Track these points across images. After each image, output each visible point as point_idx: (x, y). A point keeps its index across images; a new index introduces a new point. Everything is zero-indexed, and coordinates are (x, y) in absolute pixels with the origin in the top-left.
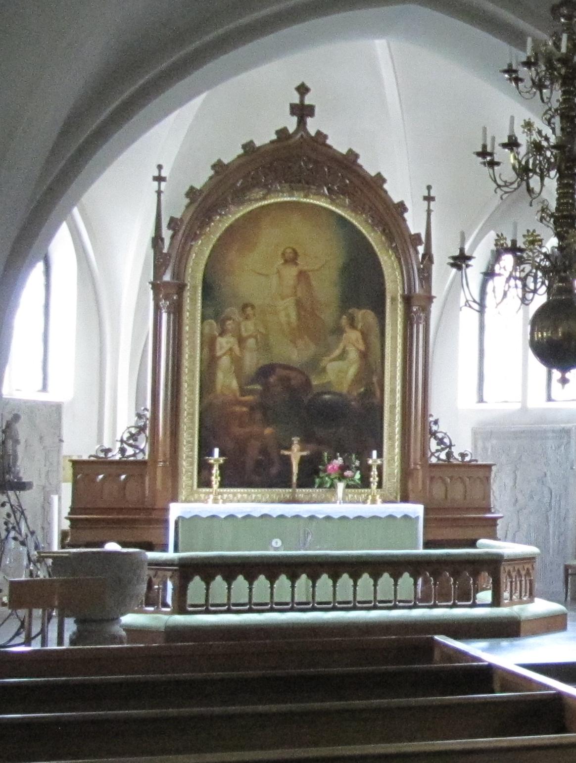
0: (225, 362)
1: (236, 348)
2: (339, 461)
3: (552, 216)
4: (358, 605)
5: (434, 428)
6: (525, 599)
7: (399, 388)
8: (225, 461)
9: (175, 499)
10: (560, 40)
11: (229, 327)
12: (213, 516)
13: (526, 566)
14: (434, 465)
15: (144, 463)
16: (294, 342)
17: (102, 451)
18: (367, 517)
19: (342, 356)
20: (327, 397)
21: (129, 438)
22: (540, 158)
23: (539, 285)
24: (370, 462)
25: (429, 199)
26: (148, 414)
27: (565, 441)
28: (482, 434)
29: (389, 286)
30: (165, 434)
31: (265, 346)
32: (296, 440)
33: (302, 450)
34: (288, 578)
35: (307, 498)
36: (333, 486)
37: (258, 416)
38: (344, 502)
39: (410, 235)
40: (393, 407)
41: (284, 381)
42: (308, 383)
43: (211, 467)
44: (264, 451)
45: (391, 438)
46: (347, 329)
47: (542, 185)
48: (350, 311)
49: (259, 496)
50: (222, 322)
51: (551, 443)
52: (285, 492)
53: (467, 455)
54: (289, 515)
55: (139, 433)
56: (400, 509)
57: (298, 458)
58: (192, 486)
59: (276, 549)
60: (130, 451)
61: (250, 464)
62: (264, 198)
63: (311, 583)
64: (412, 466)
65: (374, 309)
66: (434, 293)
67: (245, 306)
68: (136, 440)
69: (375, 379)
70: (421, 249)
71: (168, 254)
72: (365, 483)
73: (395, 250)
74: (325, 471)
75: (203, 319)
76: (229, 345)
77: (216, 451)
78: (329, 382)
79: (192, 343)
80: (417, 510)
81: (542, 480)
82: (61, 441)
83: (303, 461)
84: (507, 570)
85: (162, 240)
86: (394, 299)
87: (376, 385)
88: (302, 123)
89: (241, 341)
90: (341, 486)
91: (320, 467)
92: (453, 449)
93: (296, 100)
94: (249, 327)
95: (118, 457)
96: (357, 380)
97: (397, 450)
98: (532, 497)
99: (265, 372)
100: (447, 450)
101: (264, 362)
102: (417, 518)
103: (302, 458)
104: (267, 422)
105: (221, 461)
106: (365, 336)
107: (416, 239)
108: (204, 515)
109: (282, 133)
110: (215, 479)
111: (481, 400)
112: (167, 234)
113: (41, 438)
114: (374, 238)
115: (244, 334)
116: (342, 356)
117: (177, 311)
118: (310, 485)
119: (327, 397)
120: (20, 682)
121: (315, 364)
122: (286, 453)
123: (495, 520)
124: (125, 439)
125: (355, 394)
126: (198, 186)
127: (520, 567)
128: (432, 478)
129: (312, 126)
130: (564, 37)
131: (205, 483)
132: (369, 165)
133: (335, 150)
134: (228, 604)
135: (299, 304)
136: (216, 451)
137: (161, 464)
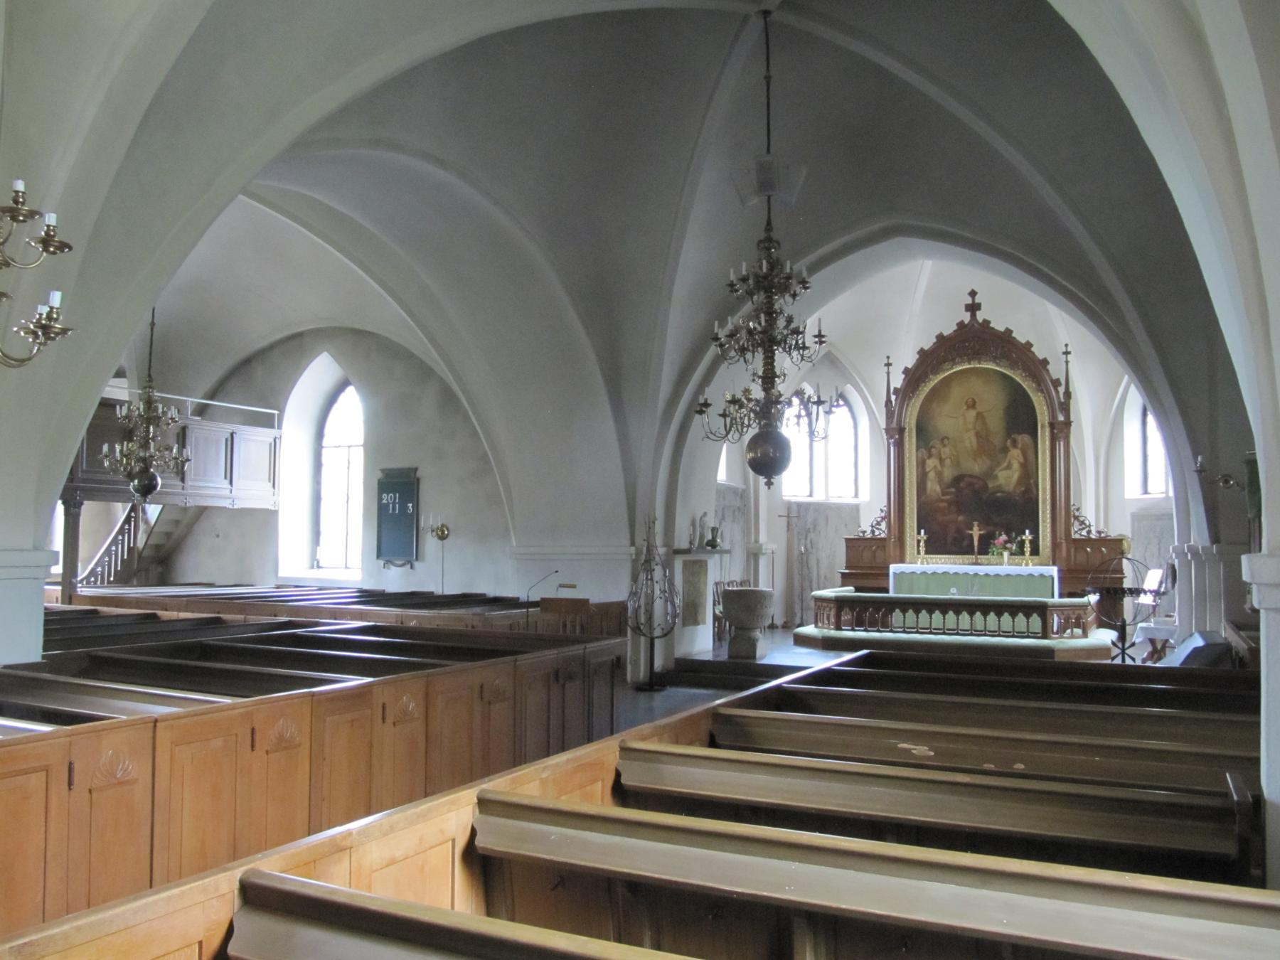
0: (932, 475)
3: (759, 377)
4: (987, 633)
5: (1077, 514)
8: (927, 538)
9: (902, 561)
10: (762, 264)
12: (913, 573)
14: (1075, 540)
16: (975, 460)
18: (992, 574)
19: (1009, 467)
22: (800, 339)
23: (752, 422)
28: (1138, 518)
30: (895, 520)
31: (956, 463)
33: (980, 530)
34: (1039, 616)
36: (1002, 554)
38: (1010, 564)
41: (970, 485)
42: (986, 486)
44: (959, 531)
46: (1011, 449)
47: (753, 357)
48: (1013, 436)
50: (929, 451)
52: (972, 558)
55: (882, 521)
58: (914, 553)
59: (953, 594)
60: (877, 533)
61: (949, 540)
62: (952, 368)
63: (956, 618)
64: (1058, 540)
65: (1029, 434)
66: (1072, 419)
67: (942, 440)
68: (880, 525)
69: (1032, 481)
70: (1062, 390)
73: (1042, 391)
77: (1027, 532)
83: (981, 537)
86: (1043, 426)
87: (1033, 485)
88: (973, 316)
89: (941, 460)
90: (1006, 554)
93: (969, 301)
94: (946, 451)
95: (869, 536)
96: (1020, 482)
99: (958, 480)
100: (1088, 529)
101: (956, 474)
103: (980, 535)
104: (960, 512)
105: (925, 538)
106: (1024, 453)
107: (1056, 383)
109: (961, 325)
110: (922, 549)
111: (1146, 492)
112: (893, 398)
113: (846, 525)
114: (1028, 386)
115: (943, 457)
116: (1009, 467)
117: (900, 445)
118: (986, 553)
119: (999, 494)
120: (864, 671)
121: (990, 474)
122: (970, 532)
125: (1018, 491)
126: (910, 366)
129: (980, 316)
130: (764, 262)
132: (1020, 336)
133: (996, 330)
134: (904, 627)
135: (978, 435)
136: (1027, 532)
137: (893, 540)
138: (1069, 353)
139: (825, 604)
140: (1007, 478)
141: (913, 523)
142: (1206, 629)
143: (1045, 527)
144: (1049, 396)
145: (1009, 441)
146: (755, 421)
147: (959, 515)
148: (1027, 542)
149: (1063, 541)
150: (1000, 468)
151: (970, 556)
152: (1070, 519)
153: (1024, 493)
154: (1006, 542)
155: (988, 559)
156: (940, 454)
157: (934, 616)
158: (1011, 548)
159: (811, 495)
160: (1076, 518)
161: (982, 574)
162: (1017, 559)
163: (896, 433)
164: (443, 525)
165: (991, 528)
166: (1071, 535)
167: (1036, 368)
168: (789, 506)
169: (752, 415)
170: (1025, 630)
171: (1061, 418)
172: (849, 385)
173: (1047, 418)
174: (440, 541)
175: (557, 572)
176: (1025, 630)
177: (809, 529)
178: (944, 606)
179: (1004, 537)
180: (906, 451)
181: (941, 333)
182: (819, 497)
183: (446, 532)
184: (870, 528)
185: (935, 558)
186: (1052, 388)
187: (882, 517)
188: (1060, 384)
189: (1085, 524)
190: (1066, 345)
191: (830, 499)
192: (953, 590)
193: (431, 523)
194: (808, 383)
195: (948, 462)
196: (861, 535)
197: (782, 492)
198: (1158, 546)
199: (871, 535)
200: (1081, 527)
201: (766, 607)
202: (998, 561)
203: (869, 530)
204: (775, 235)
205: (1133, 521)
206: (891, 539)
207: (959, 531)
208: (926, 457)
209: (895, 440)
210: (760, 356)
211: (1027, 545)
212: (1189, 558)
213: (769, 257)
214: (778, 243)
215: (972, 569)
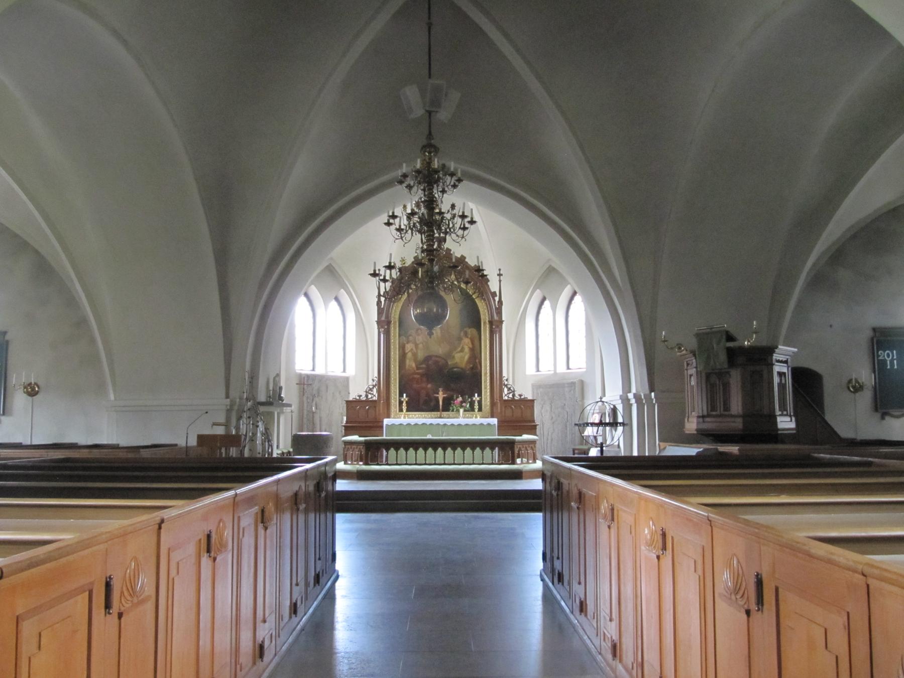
0: (409, 355)
1: (414, 349)
2: (460, 399)
5: (506, 383)
6: (531, 462)
7: (488, 364)
9: (388, 417)
11: (411, 339)
12: (401, 424)
13: (531, 446)
14: (505, 401)
15: (375, 401)
17: (358, 396)
20: (455, 369)
21: (369, 390)
24: (474, 399)
25: (500, 275)
26: (376, 379)
27: (573, 388)
28: (536, 387)
29: (482, 317)
30: (383, 387)
32: (441, 389)
33: (443, 394)
35: (453, 417)
36: (458, 411)
37: (424, 379)
38: (464, 418)
39: (491, 292)
40: (486, 374)
41: (436, 362)
43: (402, 402)
44: (428, 395)
45: (486, 388)
46: (464, 338)
49: (426, 415)
50: (408, 338)
51: (567, 389)
53: (522, 395)
54: (434, 423)
56: (486, 421)
57: (442, 398)
58: (396, 411)
60: (370, 396)
61: (421, 401)
64: (495, 400)
66: (503, 319)
68: (372, 391)
69: (477, 361)
70: (497, 299)
71: (384, 308)
72: (472, 409)
73: (484, 300)
74: (454, 404)
75: (400, 336)
76: (411, 347)
78: (456, 363)
79: (395, 347)
80: (494, 421)
81: (563, 407)
82: (349, 393)
83: (444, 399)
84: (519, 446)
85: (381, 302)
86: (485, 323)
89: (416, 345)
90: (461, 410)
91: (452, 402)
92: (515, 393)
95: (364, 399)
96: (469, 362)
97: (488, 394)
98: (559, 416)
99: (427, 359)
101: (426, 355)
102: (495, 424)
104: (428, 382)
105: (407, 400)
107: (494, 294)
108: (397, 424)
110: (404, 408)
111: (538, 371)
112: (383, 299)
115: (418, 342)
116: (462, 351)
117: (387, 334)
119: (455, 369)
121: (450, 355)
122: (438, 395)
123: (536, 425)
124: (367, 391)
125: (468, 367)
127: (527, 446)
128: (506, 407)
131: (401, 410)
137: (382, 402)
138: (502, 275)
139: (355, 446)
140: (461, 358)
141: (396, 389)
142: (655, 453)
143: (486, 392)
144: (489, 304)
145: (462, 332)
148: (476, 402)
149: (498, 401)
150: (457, 351)
151: (435, 413)
152: (502, 387)
153: (472, 368)
154: (462, 402)
155: (448, 414)
157: (466, 452)
158: (466, 406)
159: (313, 370)
161: (449, 424)
162: (468, 414)
163: (384, 323)
164: (35, 384)
165: (451, 393)
166: (502, 397)
168: (300, 376)
171: (496, 317)
172: (342, 290)
174: (29, 398)
175: (207, 413)
177: (315, 395)
179: (460, 399)
180: (392, 337)
182: (319, 371)
183: (37, 389)
184: (365, 393)
185: (411, 414)
186: (492, 299)
187: (373, 385)
188: (496, 296)
189: (511, 390)
190: (500, 270)
191: (329, 373)
193: (23, 381)
194: (316, 286)
196: (358, 398)
199: (365, 398)
201: (329, 446)
202: (455, 416)
203: (364, 395)
205: (533, 389)
206: (380, 401)
207: (428, 395)
209: (384, 330)
211: (476, 404)
212: (654, 402)
215: (441, 421)
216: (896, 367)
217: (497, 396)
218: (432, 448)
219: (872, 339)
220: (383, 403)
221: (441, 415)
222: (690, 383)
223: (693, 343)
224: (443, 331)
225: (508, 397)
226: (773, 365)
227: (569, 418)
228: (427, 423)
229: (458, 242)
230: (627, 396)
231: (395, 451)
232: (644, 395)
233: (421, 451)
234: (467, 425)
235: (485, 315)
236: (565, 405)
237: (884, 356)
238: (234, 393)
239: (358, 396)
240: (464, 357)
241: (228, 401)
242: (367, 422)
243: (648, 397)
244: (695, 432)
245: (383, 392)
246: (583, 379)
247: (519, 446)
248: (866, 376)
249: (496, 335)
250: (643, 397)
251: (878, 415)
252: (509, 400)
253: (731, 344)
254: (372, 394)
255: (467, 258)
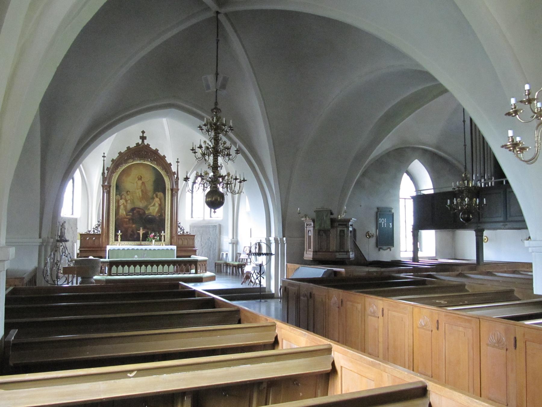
0: (122, 207)
2: (153, 234)
4: (136, 274)
5: (179, 225)
6: (204, 272)
7: (169, 214)
10: (214, 118)
11: (123, 197)
12: (119, 249)
15: (100, 234)
16: (141, 201)
17: (88, 231)
18: (152, 249)
20: (150, 216)
21: (95, 228)
24: (162, 234)
25: (178, 162)
26: (101, 221)
27: (215, 228)
28: (192, 227)
29: (167, 186)
30: (105, 227)
31: (133, 202)
32: (141, 228)
36: (151, 241)
37: (131, 222)
38: (155, 245)
40: (168, 219)
41: (138, 212)
42: (144, 213)
44: (133, 231)
46: (155, 198)
47: (209, 158)
48: (156, 193)
50: (121, 196)
52: (138, 243)
55: (98, 226)
58: (113, 241)
59: (136, 258)
60: (96, 231)
61: (129, 235)
62: (133, 162)
64: (173, 235)
66: (179, 188)
67: (127, 192)
68: (97, 228)
69: (163, 212)
70: (176, 176)
71: (106, 177)
72: (160, 240)
73: (169, 176)
74: (149, 237)
75: (116, 195)
76: (123, 202)
77: (120, 231)
80: (174, 247)
81: (209, 239)
82: (77, 228)
83: (143, 234)
85: (105, 173)
86: (168, 190)
87: (163, 213)
88: (143, 141)
89: (126, 201)
90: (154, 241)
91: (148, 236)
93: (141, 135)
94: (128, 197)
95: (93, 233)
96: (158, 212)
97: (169, 231)
98: (206, 244)
99: (133, 210)
101: (133, 207)
104: (133, 223)
106: (160, 200)
107: (174, 173)
109: (138, 144)
110: (119, 239)
111: (192, 217)
112: (106, 172)
113: (72, 228)
114: (163, 173)
115: (127, 199)
116: (154, 205)
117: (109, 193)
118: (145, 240)
119: (150, 216)
120: (66, 295)
121: (146, 207)
122: (139, 232)
123: (196, 250)
124: (94, 228)
125: (157, 215)
128: (179, 239)
129: (146, 142)
130: (215, 118)
132: (162, 153)
134: (123, 273)
135: (142, 191)
136: (120, 231)
137: (104, 235)
140: (153, 210)
145: (155, 194)
146: (209, 185)
147: (133, 225)
154: (154, 236)
156: (126, 198)
160: (179, 227)
167: (167, 167)
169: (208, 183)
170: (139, 272)
173: (170, 187)
176: (139, 272)
178: (135, 263)
181: (129, 146)
189: (182, 229)
190: (178, 159)
192: (136, 256)
195: (129, 201)
196: (88, 232)
197: (60, 212)
198: (201, 238)
200: (180, 230)
204: (218, 107)
208: (120, 199)
210: (211, 158)
211: (163, 237)
213: (216, 116)
214: (220, 109)
215: (143, 247)
216: (385, 226)
217: (174, 232)
218: (139, 265)
219: (377, 213)
220: (105, 235)
221: (141, 243)
222: (308, 234)
223: (314, 215)
224: (143, 193)
225: (180, 233)
226: (349, 227)
227: (212, 245)
228: (135, 248)
229: (227, 162)
230: (269, 239)
231: (134, 267)
232: (280, 239)
233: (149, 267)
234: (159, 249)
235: (168, 185)
236: (210, 238)
237: (381, 221)
238: (44, 235)
239: (88, 231)
240: (155, 210)
241: (41, 240)
242: (94, 247)
243: (282, 240)
244: (312, 259)
245: (105, 228)
246: (220, 224)
247: (199, 263)
248: (373, 230)
249: (175, 197)
250: (279, 240)
251: (377, 249)
252: (181, 235)
253: (332, 217)
254: (98, 230)
255: (159, 151)
